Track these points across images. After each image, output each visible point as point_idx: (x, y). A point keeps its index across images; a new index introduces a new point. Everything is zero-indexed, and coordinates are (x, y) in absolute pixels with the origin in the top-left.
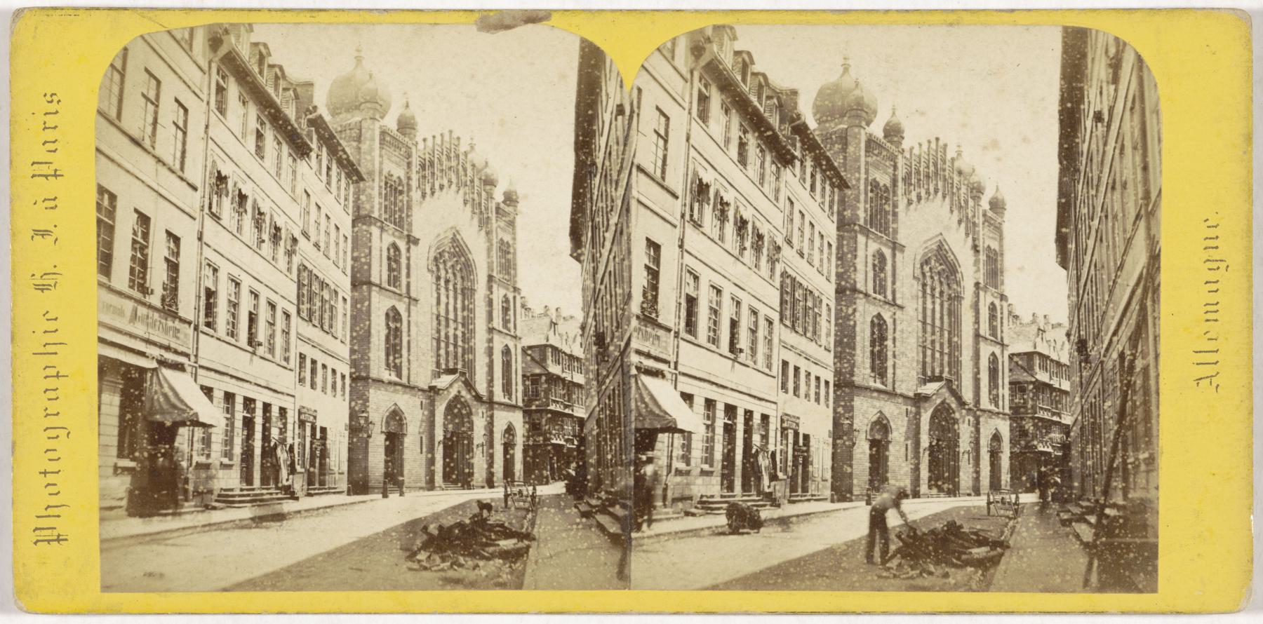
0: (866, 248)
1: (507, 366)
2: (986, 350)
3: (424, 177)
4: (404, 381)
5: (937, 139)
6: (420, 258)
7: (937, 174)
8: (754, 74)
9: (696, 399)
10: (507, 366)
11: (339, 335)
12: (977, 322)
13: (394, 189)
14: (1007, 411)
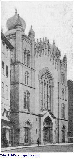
1: (63, 108)
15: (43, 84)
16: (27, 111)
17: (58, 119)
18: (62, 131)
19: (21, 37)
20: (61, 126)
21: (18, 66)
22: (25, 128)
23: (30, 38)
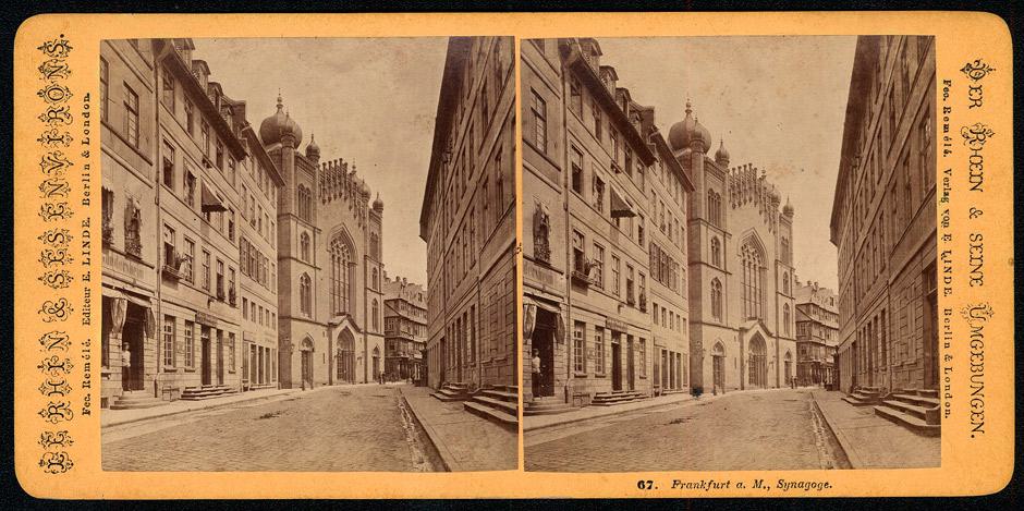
0: (707, 235)
1: (375, 311)
4: (313, 319)
5: (750, 165)
6: (733, 247)
7: (752, 187)
9: (177, 320)
11: (681, 293)
12: (365, 280)
17: (778, 337)
18: (715, 357)
20: (782, 354)
23: (720, 167)
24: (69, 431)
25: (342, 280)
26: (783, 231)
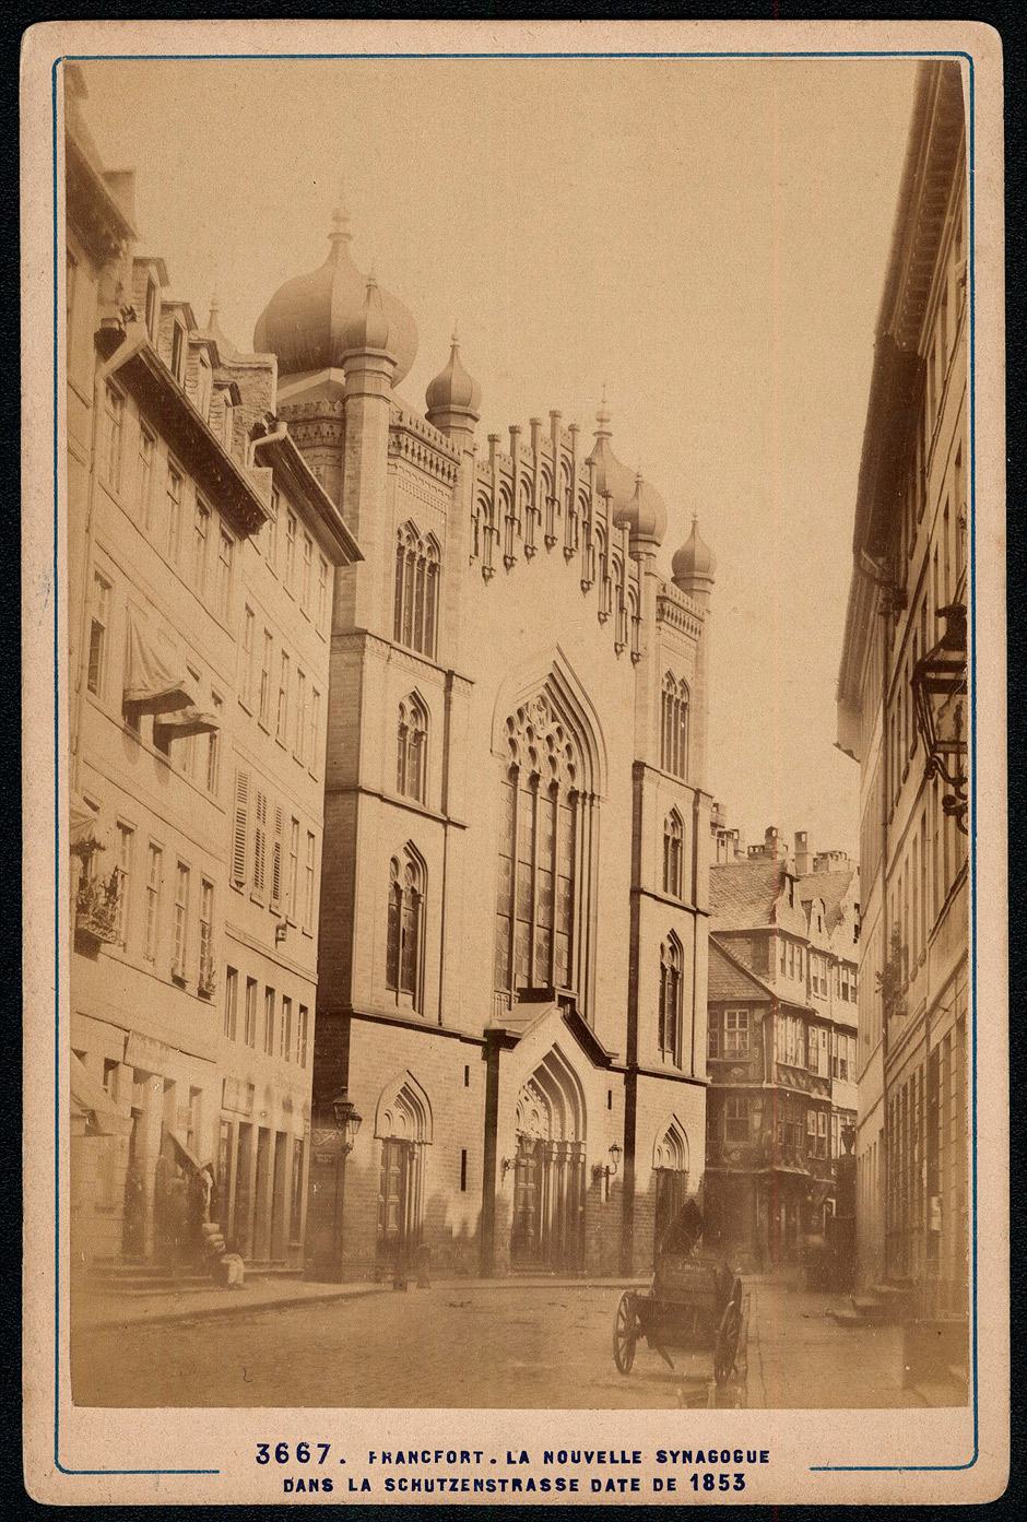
0: (388, 682)
1: (672, 979)
2: (658, 921)
3: (490, 529)
4: (430, 1017)
8: (167, 308)
10: (672, 979)
13: (420, 565)
14: (701, 1073)
15: (523, 778)
16: (404, 1007)
19: (384, 437)
21: (355, 658)
22: (386, 1141)
24: (74, 1445)
25: (543, 859)
26: (664, 647)
